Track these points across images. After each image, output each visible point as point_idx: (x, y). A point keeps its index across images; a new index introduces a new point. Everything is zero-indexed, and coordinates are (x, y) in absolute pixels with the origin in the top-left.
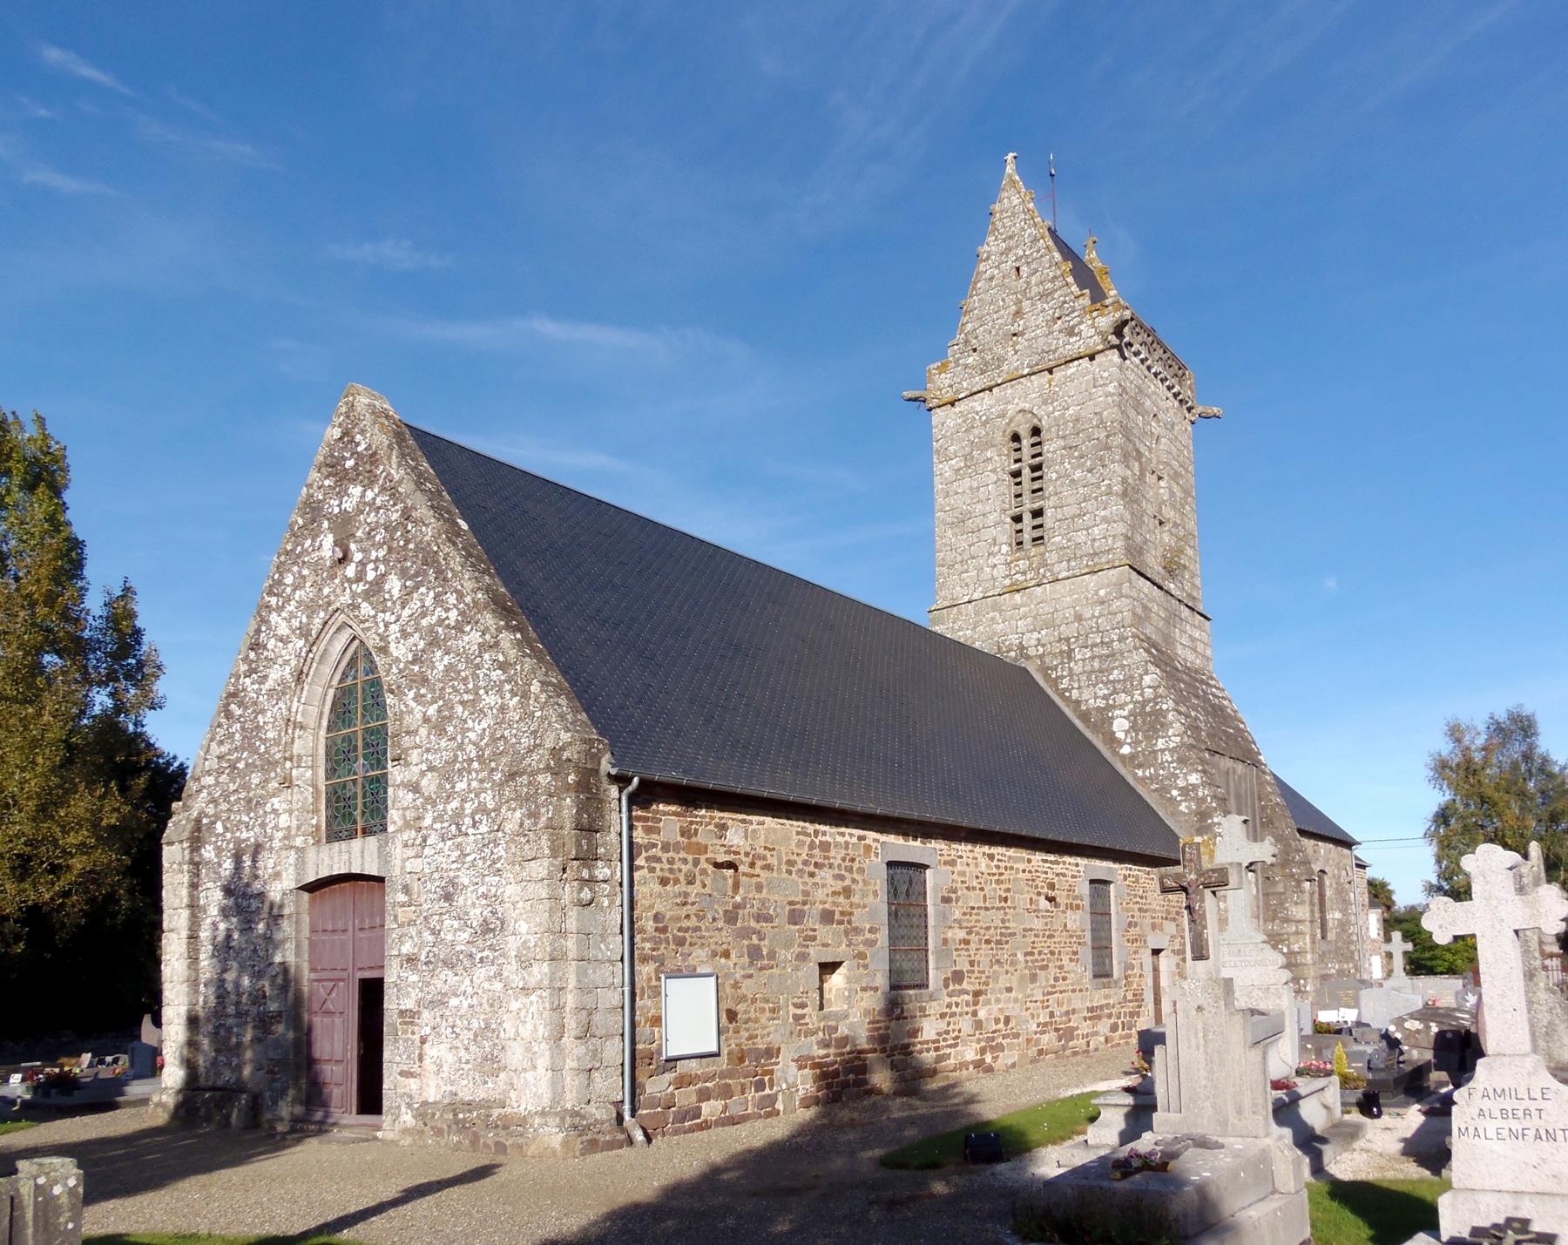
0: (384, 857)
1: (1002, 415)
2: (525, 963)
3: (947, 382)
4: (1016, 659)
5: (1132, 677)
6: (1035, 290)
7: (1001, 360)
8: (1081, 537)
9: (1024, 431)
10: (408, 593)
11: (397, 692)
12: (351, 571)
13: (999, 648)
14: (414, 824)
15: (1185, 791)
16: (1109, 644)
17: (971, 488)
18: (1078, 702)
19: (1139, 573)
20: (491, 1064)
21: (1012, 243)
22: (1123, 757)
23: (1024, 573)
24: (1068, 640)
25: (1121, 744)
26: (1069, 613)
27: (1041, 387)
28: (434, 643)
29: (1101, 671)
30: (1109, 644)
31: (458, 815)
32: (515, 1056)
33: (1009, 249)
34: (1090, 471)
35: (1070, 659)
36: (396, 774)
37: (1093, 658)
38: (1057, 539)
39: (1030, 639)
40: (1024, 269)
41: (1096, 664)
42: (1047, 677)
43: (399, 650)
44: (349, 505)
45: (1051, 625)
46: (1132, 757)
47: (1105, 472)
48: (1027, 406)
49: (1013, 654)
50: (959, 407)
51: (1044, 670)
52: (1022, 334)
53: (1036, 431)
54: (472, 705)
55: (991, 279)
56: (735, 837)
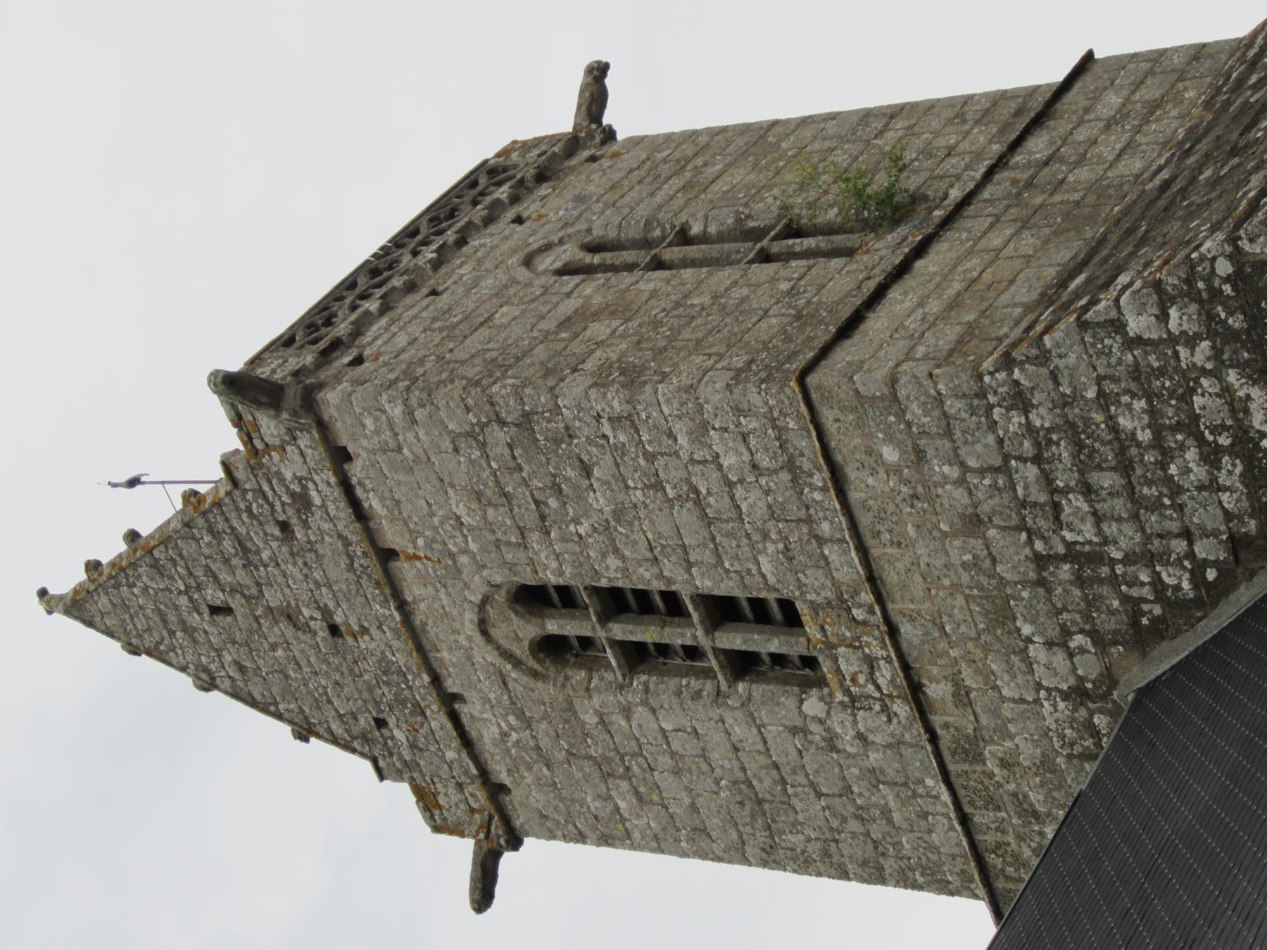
3: (455, 796)
4: (1113, 714)
5: (1136, 372)
8: (751, 501)
9: (521, 631)
13: (1088, 756)
16: (1042, 440)
17: (677, 772)
18: (1236, 544)
19: (848, 328)
21: (172, 618)
23: (871, 663)
24: (1041, 561)
26: (960, 551)
27: (424, 580)
29: (1125, 467)
30: (1042, 440)
33: (189, 631)
34: (587, 471)
35: (1097, 558)
37: (1088, 490)
38: (766, 567)
39: (1053, 668)
41: (1107, 480)
42: (1159, 631)
47: (584, 431)
48: (470, 616)
49: (1100, 721)
51: (1143, 637)
52: (326, 613)
55: (242, 669)
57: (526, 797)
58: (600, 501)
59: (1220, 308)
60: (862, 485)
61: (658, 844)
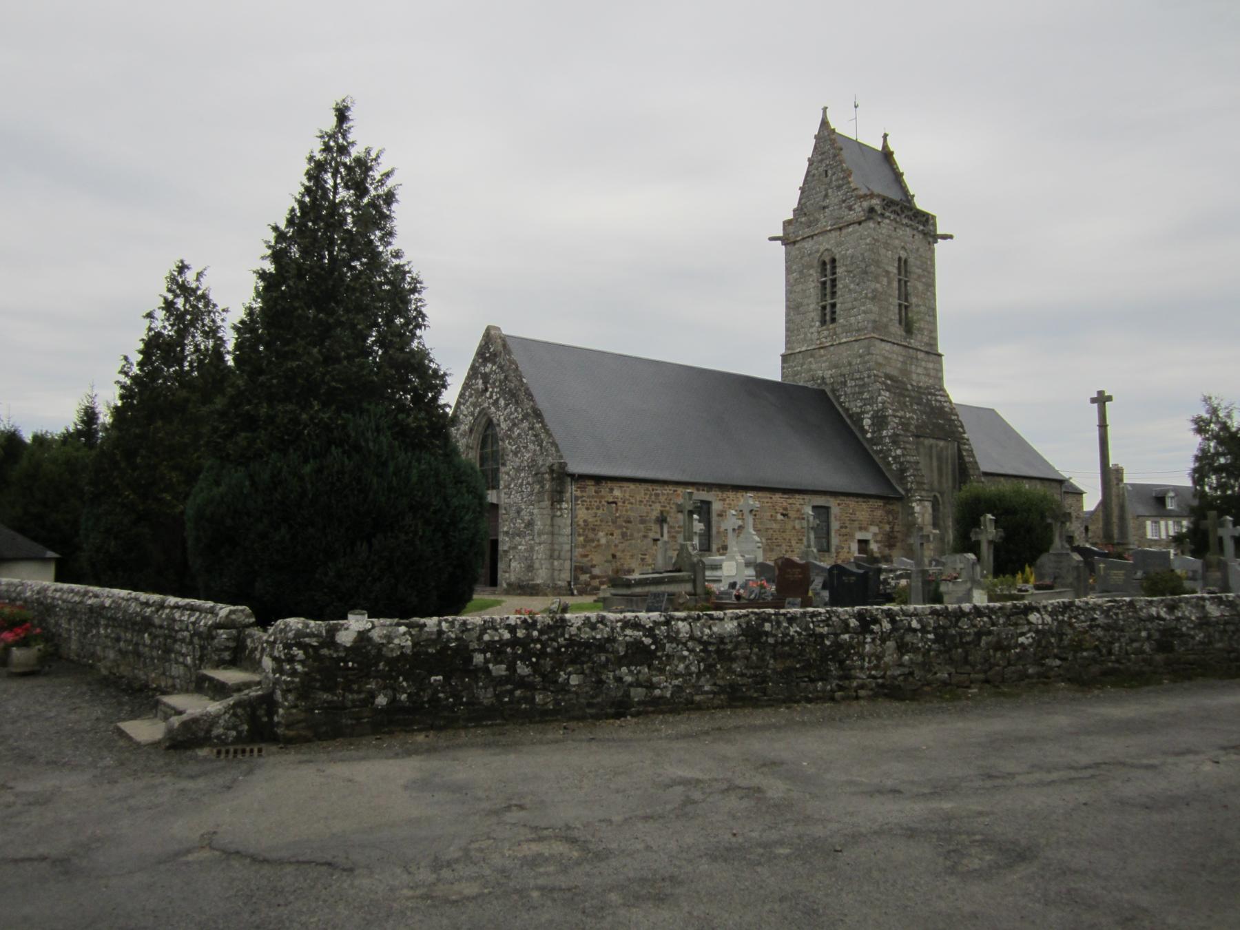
0: (499, 497)
1: (817, 251)
2: (540, 534)
6: (834, 183)
7: (817, 221)
8: (852, 320)
9: (827, 259)
10: (507, 405)
11: (503, 441)
12: (488, 394)
14: (508, 487)
15: (895, 458)
20: (530, 568)
22: (868, 439)
25: (867, 432)
28: (514, 425)
31: (521, 485)
32: (537, 565)
36: (503, 469)
39: (828, 373)
40: (830, 173)
43: (503, 426)
44: (487, 370)
45: (836, 366)
46: (871, 439)
50: (797, 246)
51: (833, 391)
53: (834, 261)
54: (526, 447)
56: (617, 493)
57: (794, 251)
58: (852, 286)
59: (433, 678)
60: (856, 345)
61: (787, 281)
